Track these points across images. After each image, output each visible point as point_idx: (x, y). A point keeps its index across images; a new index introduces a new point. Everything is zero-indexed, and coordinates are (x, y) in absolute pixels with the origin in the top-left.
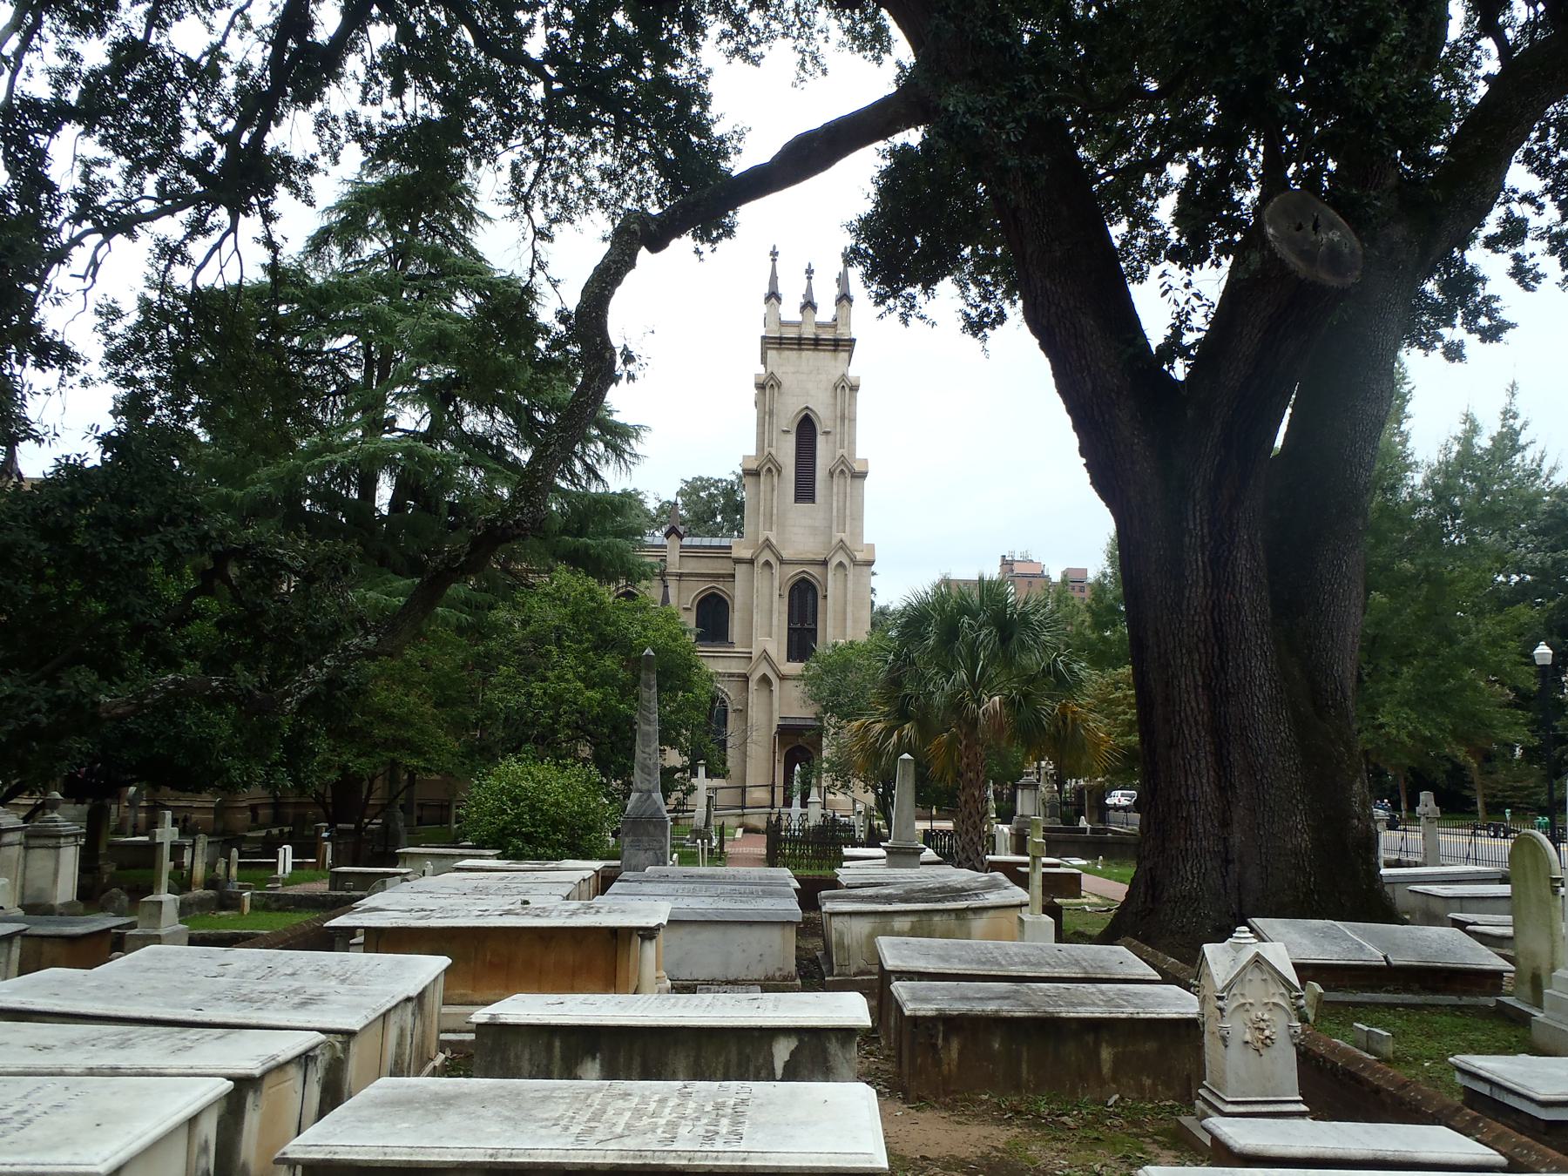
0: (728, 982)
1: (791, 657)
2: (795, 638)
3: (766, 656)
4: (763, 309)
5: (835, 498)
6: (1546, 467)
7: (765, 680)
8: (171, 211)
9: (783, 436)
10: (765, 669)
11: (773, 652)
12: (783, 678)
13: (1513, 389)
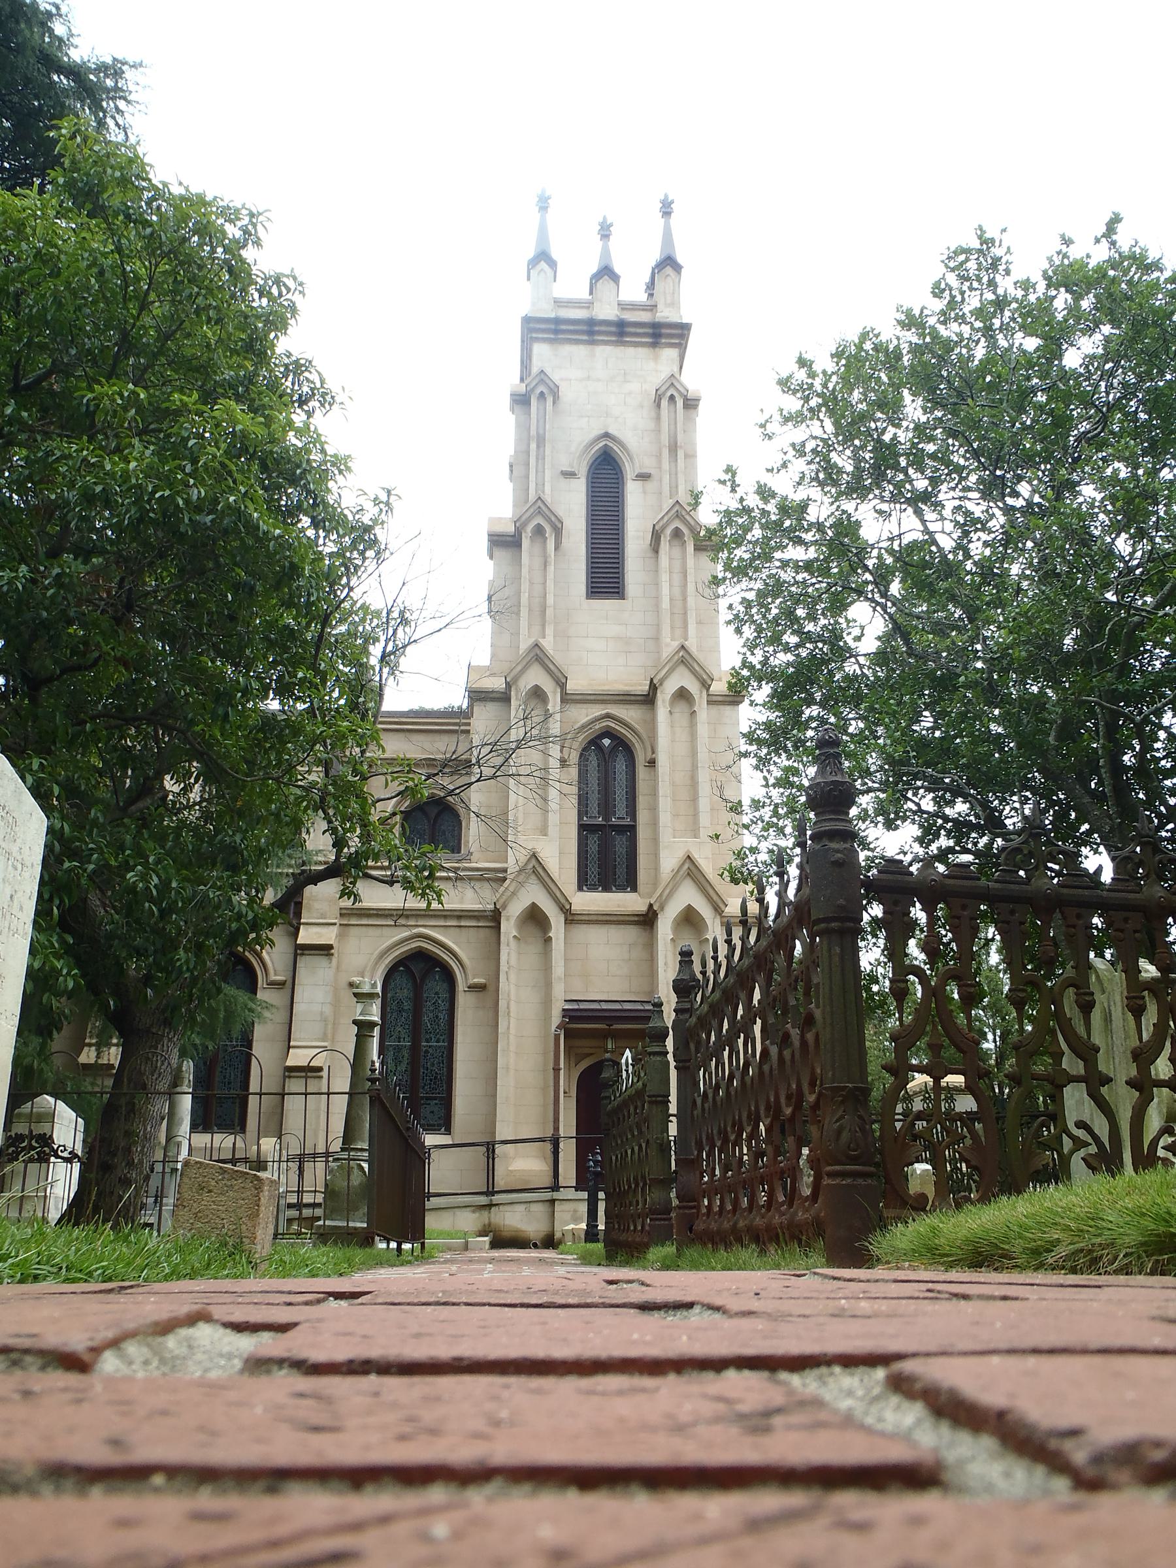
1: (584, 883)
3: (536, 868)
10: (533, 894)
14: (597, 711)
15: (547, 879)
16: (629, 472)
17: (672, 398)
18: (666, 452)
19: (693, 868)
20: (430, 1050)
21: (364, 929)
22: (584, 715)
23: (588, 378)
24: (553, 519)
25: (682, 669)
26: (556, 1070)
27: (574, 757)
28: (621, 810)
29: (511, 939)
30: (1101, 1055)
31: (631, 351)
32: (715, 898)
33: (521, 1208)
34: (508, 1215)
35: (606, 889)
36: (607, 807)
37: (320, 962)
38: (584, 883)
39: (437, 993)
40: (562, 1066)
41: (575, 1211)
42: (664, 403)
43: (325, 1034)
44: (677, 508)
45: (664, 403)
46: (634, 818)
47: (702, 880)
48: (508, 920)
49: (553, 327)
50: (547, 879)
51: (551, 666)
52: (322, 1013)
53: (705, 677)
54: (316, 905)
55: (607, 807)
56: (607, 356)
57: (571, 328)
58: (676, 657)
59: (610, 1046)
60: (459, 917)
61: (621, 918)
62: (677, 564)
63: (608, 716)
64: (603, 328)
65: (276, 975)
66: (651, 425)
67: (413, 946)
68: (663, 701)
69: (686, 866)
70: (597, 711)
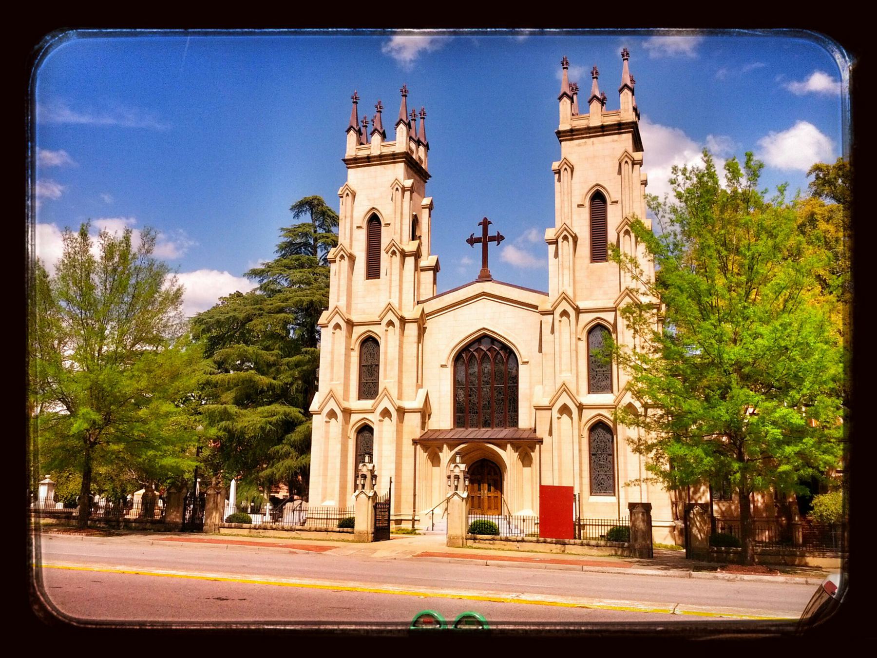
17: (347, 195)
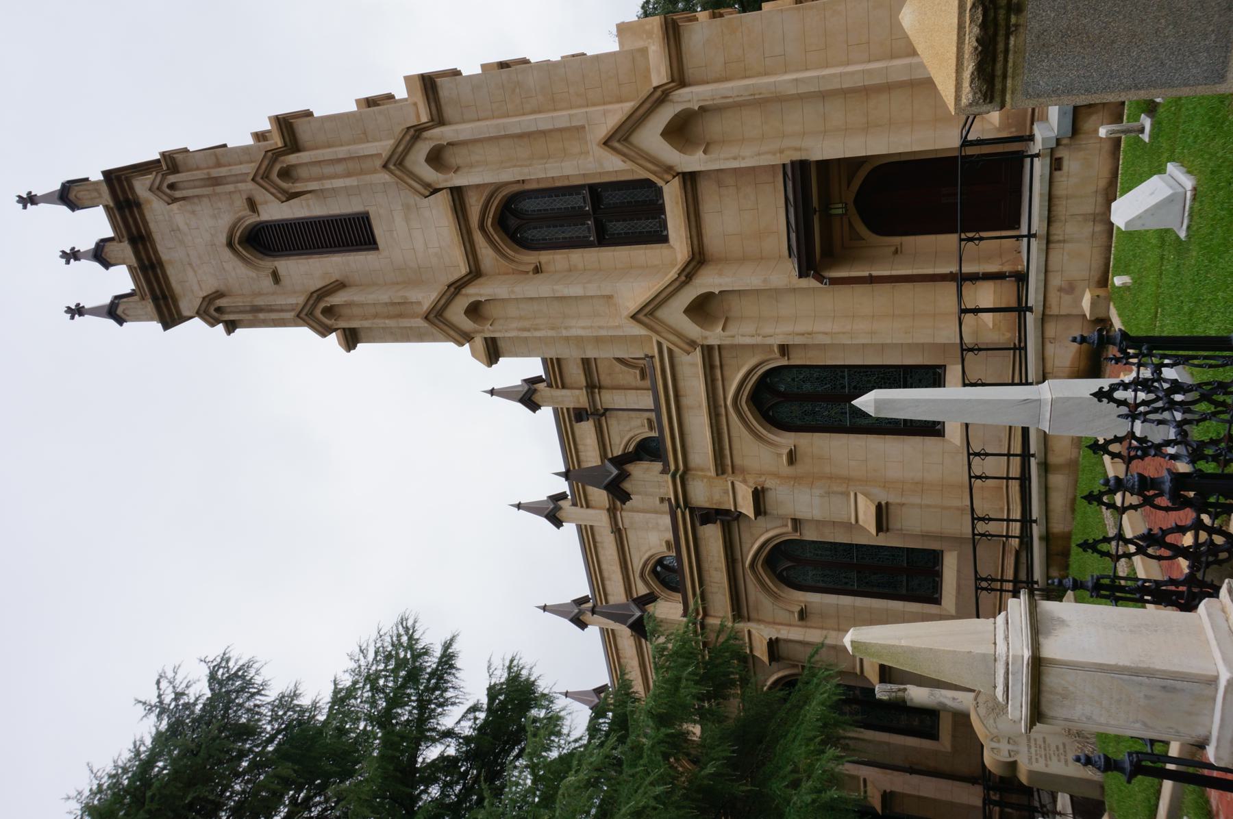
0: (1043, 359)
1: (659, 236)
2: (617, 227)
3: (647, 313)
4: (83, 261)
5: (328, 184)
6: (454, 671)
7: (702, 309)
8: (810, 794)
9: (285, 281)
10: (675, 314)
11: (635, 294)
12: (699, 259)
13: (72, 255)
14: (479, 238)
15: (656, 302)
16: (252, 219)
18: (219, 189)
19: (618, 136)
20: (853, 384)
21: (735, 452)
22: (486, 254)
23: (190, 264)
24: (311, 302)
25: (408, 163)
26: (872, 280)
27: (531, 258)
28: (576, 201)
29: (726, 333)
30: (973, 718)
31: (152, 226)
32: (647, 105)
33: (1050, 349)
34: (1057, 363)
35: (662, 209)
36: (575, 216)
37: (771, 497)
38: (659, 236)
39: (793, 380)
40: (866, 274)
41: (1060, 290)
42: (178, 194)
43: (842, 493)
44: (258, 179)
45: (178, 194)
46: (582, 187)
47: (629, 124)
48: (706, 338)
49: (162, 302)
50: (656, 302)
51: (443, 301)
52: (821, 496)
53: (408, 138)
54: (717, 497)
55: (575, 216)
56: (167, 249)
57: (155, 285)
58: (398, 172)
59: (840, 211)
60: (712, 367)
61: (690, 200)
62: (315, 171)
63: (482, 227)
64: (144, 257)
65: (787, 526)
66: (206, 200)
67: (746, 408)
68: (446, 181)
69: (616, 145)
70: (479, 238)
